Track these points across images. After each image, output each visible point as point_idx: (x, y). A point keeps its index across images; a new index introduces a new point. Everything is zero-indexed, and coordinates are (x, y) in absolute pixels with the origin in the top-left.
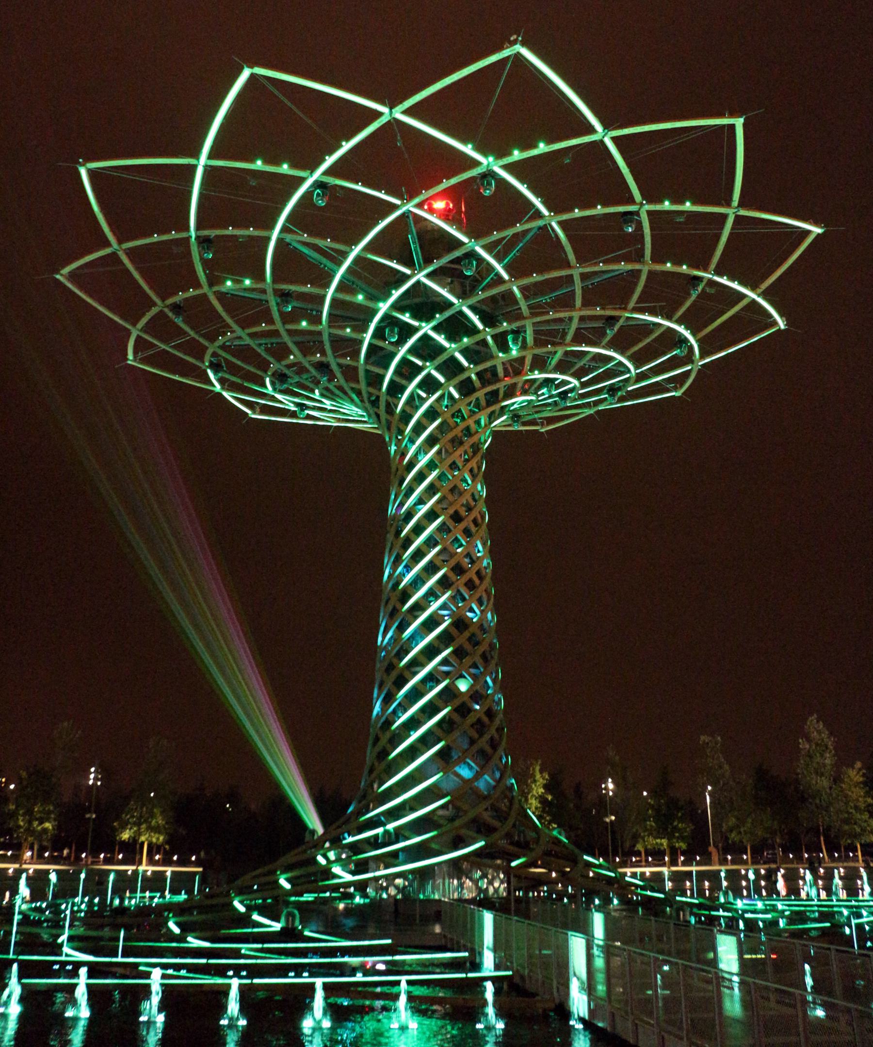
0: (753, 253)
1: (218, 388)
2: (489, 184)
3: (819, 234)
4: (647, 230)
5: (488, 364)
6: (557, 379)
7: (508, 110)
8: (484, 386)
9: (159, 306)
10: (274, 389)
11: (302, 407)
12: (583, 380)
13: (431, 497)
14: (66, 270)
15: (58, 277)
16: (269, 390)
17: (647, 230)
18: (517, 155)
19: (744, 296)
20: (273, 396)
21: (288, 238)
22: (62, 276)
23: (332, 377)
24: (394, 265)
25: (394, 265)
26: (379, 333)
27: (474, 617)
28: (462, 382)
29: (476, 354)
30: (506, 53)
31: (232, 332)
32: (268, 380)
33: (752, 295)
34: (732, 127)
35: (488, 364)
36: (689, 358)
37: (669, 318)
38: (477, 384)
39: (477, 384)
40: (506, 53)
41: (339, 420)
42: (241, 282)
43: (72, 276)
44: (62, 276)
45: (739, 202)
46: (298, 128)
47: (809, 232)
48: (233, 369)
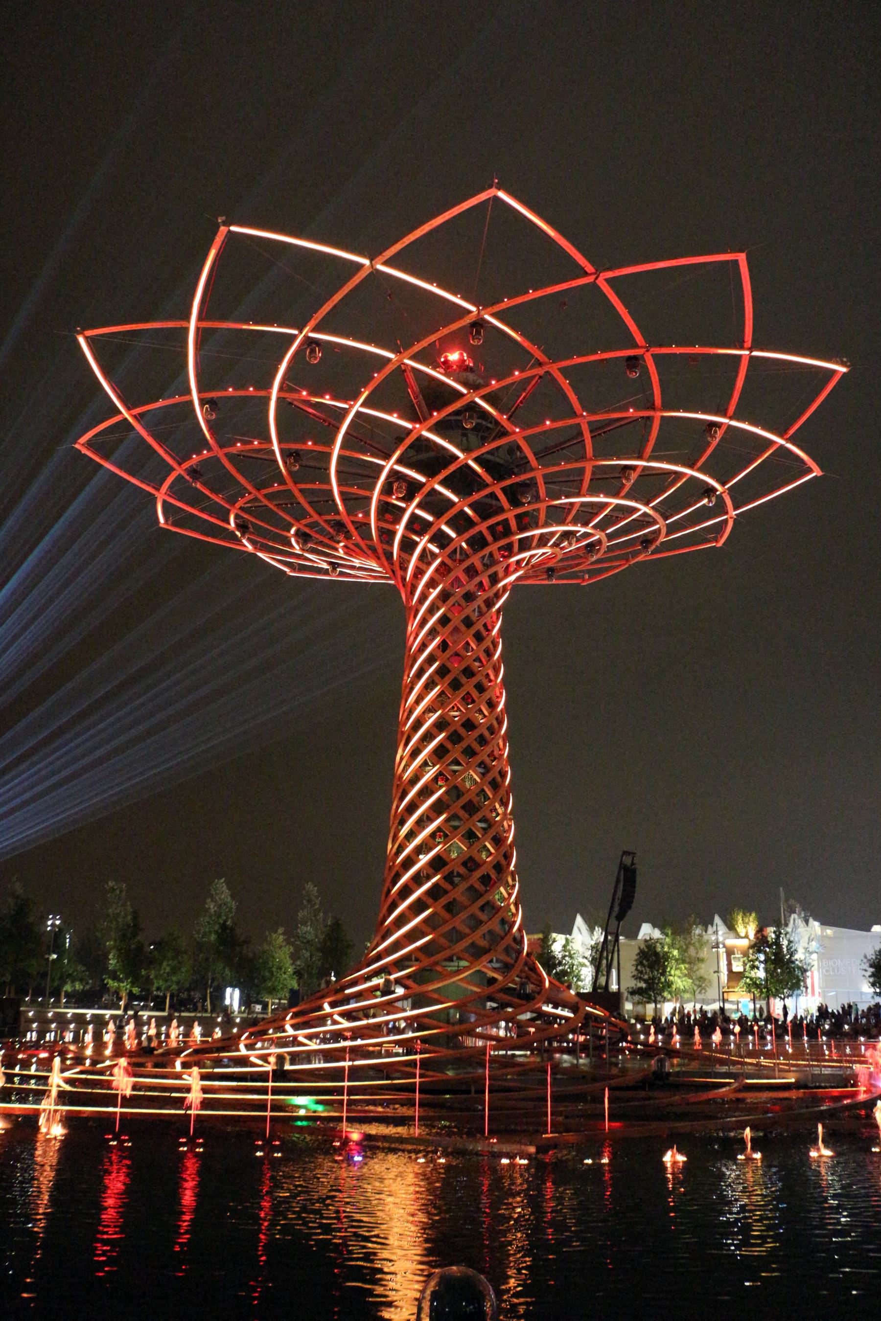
0: (773, 397)
1: (250, 548)
2: (478, 333)
3: (845, 373)
4: (655, 378)
5: (500, 518)
6: (579, 531)
7: (486, 256)
8: (496, 539)
9: (179, 471)
10: (302, 550)
11: (334, 566)
12: (608, 532)
13: (431, 666)
14: (83, 440)
15: (77, 446)
16: (297, 549)
17: (655, 378)
18: (506, 303)
19: (772, 443)
20: (302, 555)
21: (290, 397)
22: (81, 445)
23: (348, 537)
24: (394, 418)
25: (394, 418)
26: (388, 490)
27: (168, 969)
28: (472, 537)
29: (485, 510)
30: (483, 196)
31: (250, 493)
32: (293, 540)
33: (781, 441)
34: (736, 263)
35: (500, 518)
36: (720, 508)
37: (691, 466)
38: (489, 538)
39: (489, 538)
40: (483, 196)
41: (375, 577)
42: (252, 443)
43: (90, 444)
44: (81, 445)
45: (753, 340)
46: (299, 287)
47: (834, 372)
48: (259, 530)
